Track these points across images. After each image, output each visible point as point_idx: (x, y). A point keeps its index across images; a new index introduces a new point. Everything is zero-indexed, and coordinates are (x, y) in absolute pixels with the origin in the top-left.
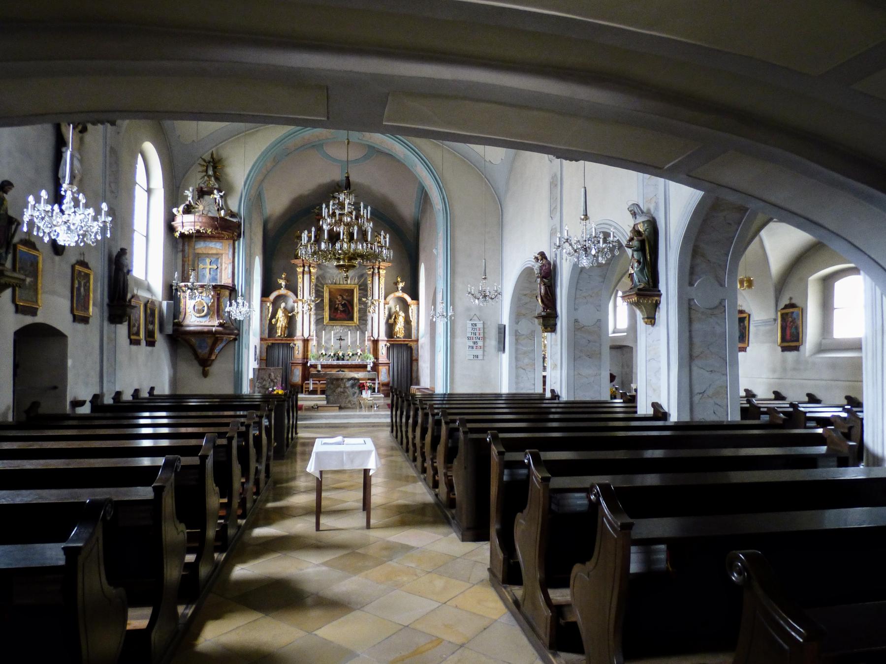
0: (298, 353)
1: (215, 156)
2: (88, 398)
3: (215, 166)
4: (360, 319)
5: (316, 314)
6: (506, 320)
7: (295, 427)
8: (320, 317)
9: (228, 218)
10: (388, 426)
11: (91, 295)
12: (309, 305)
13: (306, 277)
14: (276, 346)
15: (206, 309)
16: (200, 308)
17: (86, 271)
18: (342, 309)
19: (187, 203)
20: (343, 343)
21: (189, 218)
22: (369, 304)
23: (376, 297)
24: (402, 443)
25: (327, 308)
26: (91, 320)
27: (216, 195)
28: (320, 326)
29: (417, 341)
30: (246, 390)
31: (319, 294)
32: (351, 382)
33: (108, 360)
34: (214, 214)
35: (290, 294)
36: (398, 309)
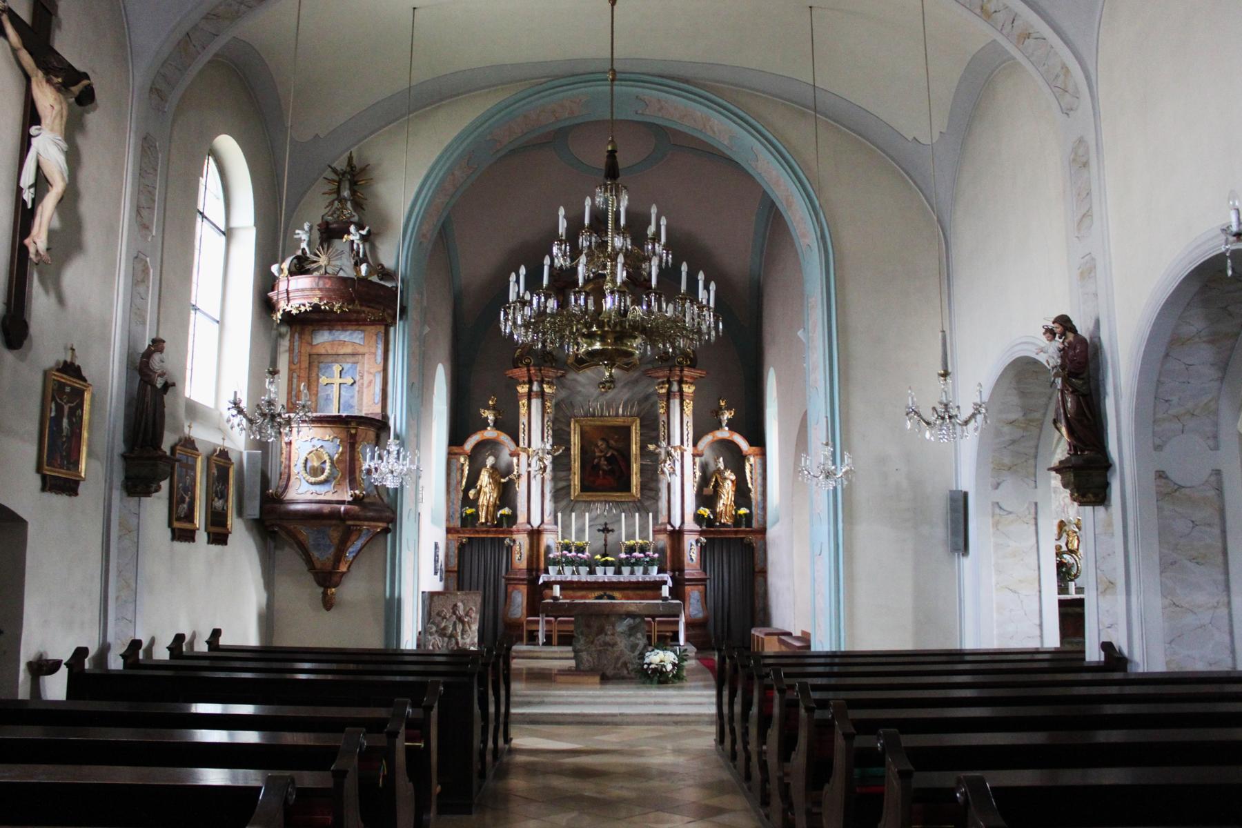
0: (520, 560)
1: (355, 162)
2: (65, 655)
3: (354, 182)
4: (644, 487)
5: (555, 479)
6: (967, 482)
7: (505, 723)
8: (562, 484)
9: (375, 279)
10: (711, 723)
11: (85, 434)
12: (541, 460)
13: (536, 403)
14: (478, 545)
15: (328, 466)
16: (316, 464)
17: (78, 384)
18: (607, 467)
19: (299, 253)
20: (611, 537)
21: (302, 282)
22: (663, 456)
23: (676, 441)
24: (748, 777)
25: (576, 466)
26: (82, 488)
27: (354, 235)
28: (563, 503)
29: (763, 531)
30: (409, 642)
31: (560, 438)
32: (629, 621)
33: (120, 572)
34: (349, 272)
35: (504, 438)
36: (721, 465)
